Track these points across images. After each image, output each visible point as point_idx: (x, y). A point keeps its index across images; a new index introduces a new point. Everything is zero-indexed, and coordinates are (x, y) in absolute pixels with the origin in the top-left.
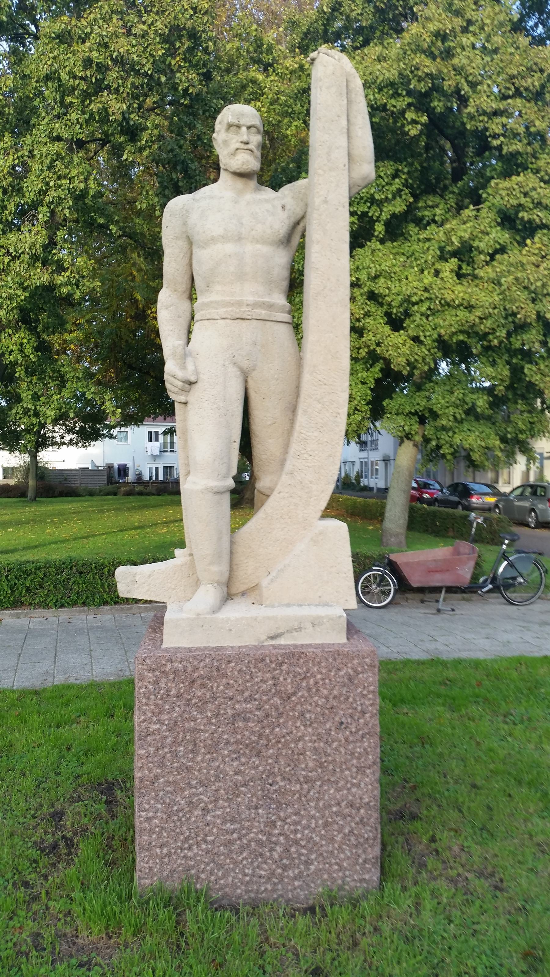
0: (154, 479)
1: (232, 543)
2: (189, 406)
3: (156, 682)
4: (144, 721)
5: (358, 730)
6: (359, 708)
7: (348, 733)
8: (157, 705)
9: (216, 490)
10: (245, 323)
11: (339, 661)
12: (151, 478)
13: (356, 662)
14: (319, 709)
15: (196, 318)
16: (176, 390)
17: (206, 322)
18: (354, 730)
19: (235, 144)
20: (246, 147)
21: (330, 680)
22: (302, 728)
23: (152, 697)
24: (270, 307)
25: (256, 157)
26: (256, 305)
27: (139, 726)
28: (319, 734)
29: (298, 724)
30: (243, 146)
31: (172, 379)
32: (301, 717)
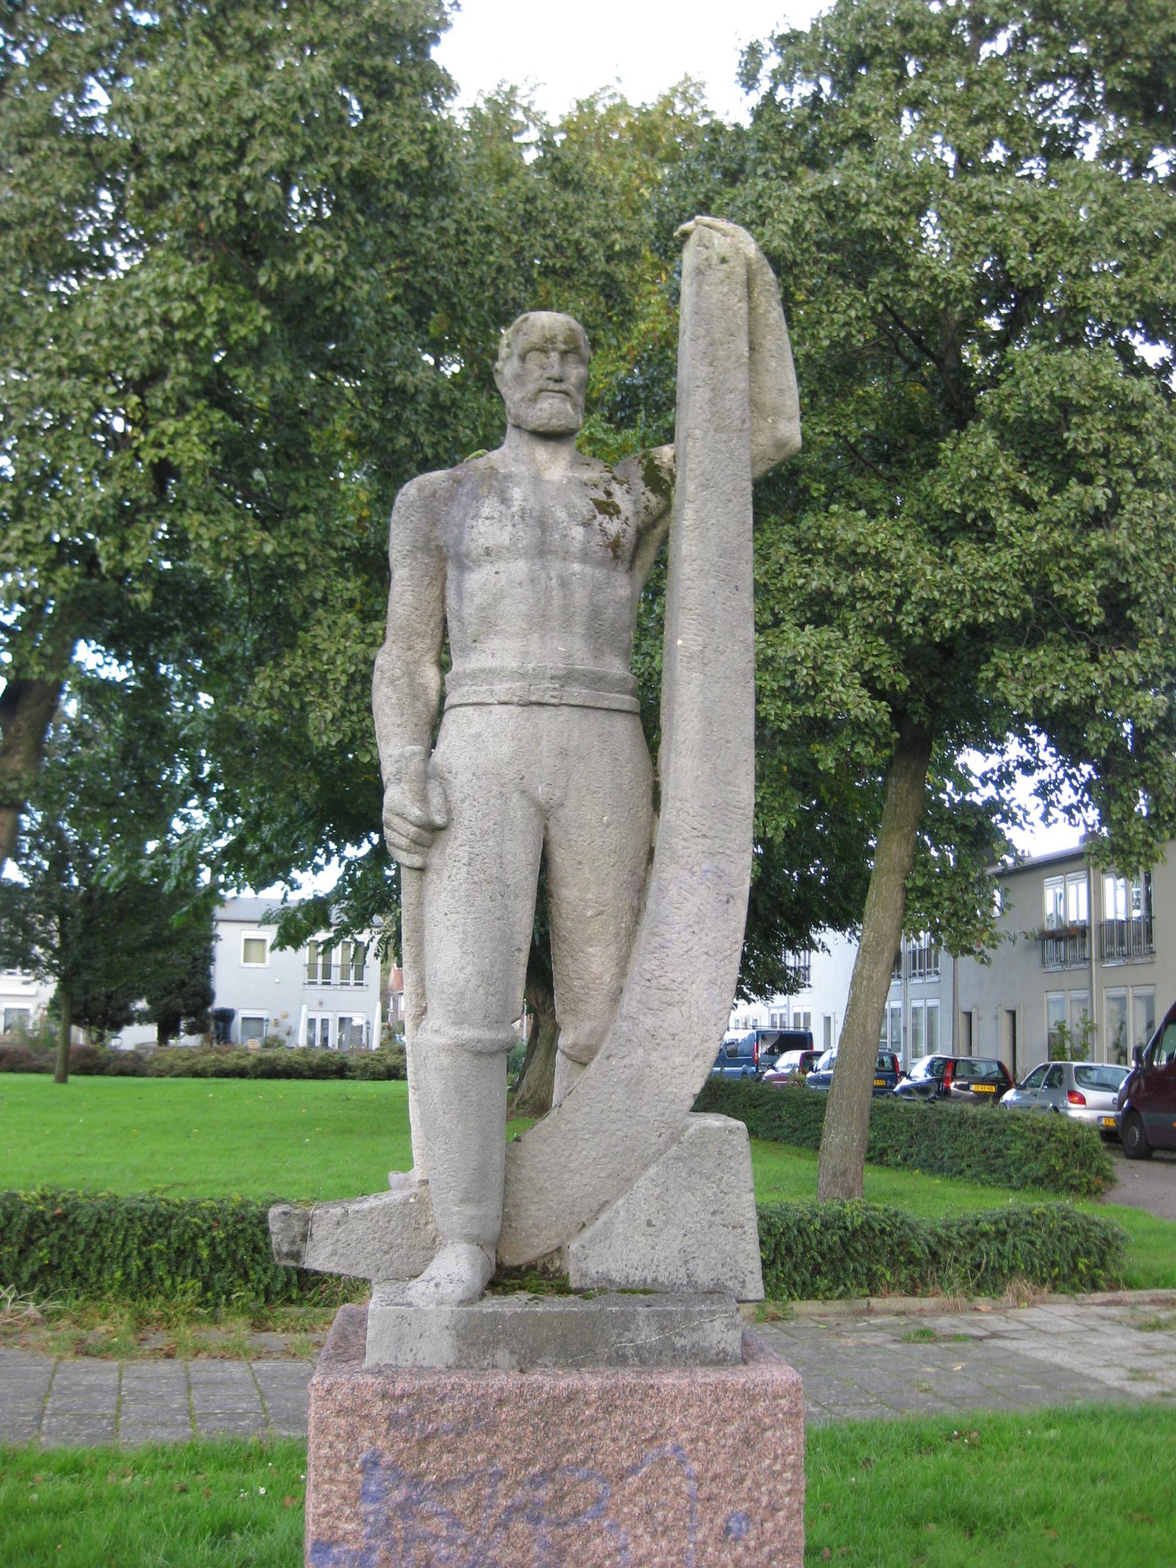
0: (318, 1043)
1: (510, 1159)
2: (431, 876)
3: (352, 1435)
4: (327, 1514)
5: (761, 1545)
6: (765, 1500)
7: (740, 1549)
8: (352, 1483)
9: (479, 1047)
10: (546, 714)
11: (726, 1403)
12: (311, 1042)
13: (761, 1406)
14: (683, 1502)
15: (447, 703)
16: (404, 842)
17: (469, 710)
18: (752, 1544)
19: (535, 377)
20: (557, 387)
21: (707, 1442)
22: (647, 1538)
23: (344, 1467)
24: (597, 681)
25: (575, 405)
26: (568, 678)
27: (317, 1523)
28: (681, 1551)
29: (639, 1531)
30: (552, 385)
31: (396, 821)
32: (646, 1518)
